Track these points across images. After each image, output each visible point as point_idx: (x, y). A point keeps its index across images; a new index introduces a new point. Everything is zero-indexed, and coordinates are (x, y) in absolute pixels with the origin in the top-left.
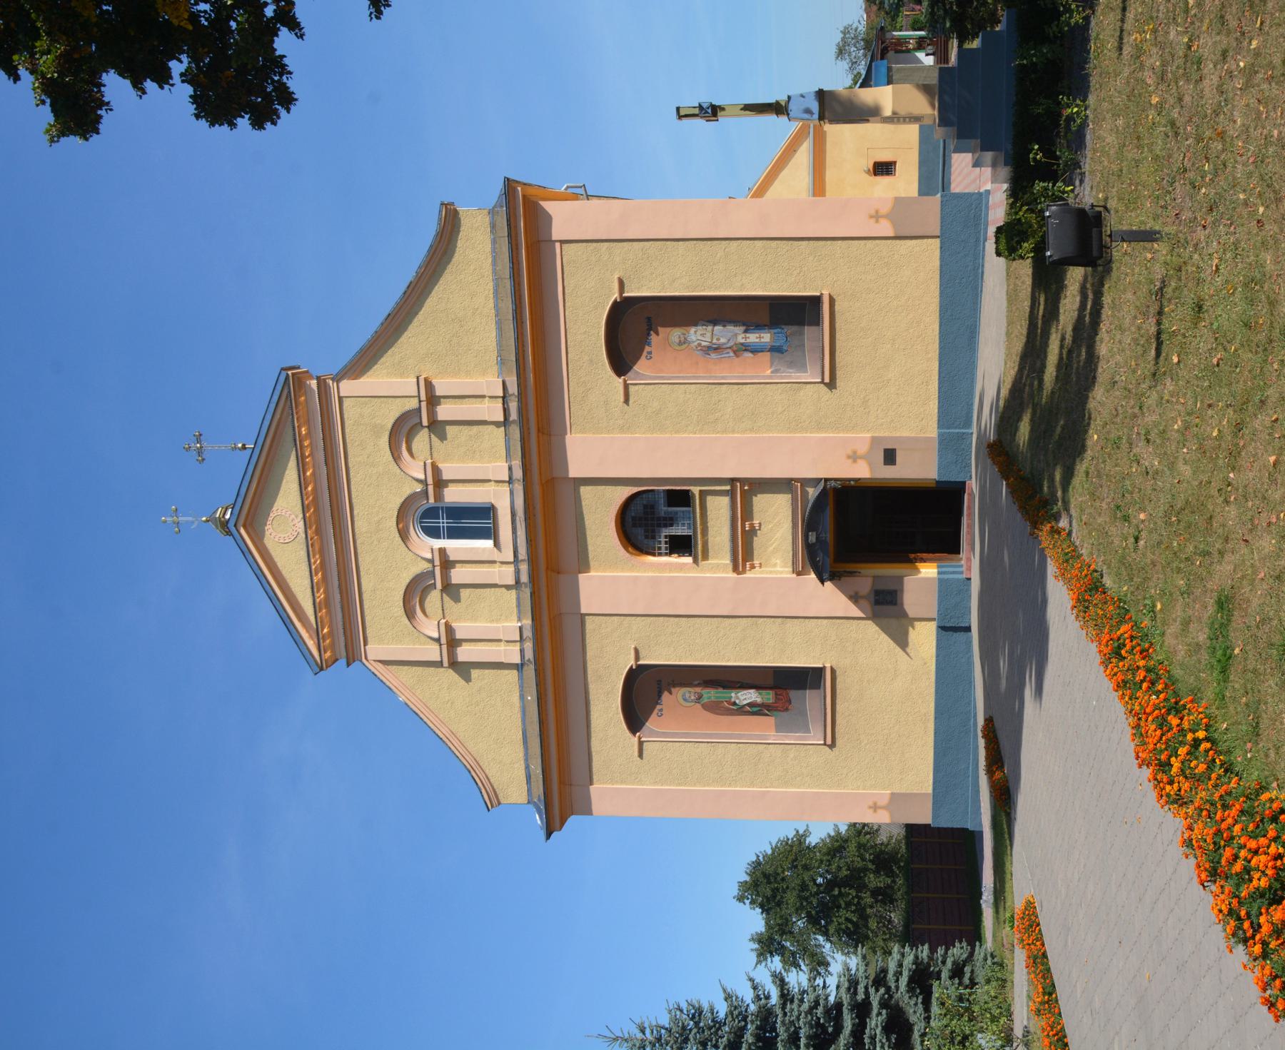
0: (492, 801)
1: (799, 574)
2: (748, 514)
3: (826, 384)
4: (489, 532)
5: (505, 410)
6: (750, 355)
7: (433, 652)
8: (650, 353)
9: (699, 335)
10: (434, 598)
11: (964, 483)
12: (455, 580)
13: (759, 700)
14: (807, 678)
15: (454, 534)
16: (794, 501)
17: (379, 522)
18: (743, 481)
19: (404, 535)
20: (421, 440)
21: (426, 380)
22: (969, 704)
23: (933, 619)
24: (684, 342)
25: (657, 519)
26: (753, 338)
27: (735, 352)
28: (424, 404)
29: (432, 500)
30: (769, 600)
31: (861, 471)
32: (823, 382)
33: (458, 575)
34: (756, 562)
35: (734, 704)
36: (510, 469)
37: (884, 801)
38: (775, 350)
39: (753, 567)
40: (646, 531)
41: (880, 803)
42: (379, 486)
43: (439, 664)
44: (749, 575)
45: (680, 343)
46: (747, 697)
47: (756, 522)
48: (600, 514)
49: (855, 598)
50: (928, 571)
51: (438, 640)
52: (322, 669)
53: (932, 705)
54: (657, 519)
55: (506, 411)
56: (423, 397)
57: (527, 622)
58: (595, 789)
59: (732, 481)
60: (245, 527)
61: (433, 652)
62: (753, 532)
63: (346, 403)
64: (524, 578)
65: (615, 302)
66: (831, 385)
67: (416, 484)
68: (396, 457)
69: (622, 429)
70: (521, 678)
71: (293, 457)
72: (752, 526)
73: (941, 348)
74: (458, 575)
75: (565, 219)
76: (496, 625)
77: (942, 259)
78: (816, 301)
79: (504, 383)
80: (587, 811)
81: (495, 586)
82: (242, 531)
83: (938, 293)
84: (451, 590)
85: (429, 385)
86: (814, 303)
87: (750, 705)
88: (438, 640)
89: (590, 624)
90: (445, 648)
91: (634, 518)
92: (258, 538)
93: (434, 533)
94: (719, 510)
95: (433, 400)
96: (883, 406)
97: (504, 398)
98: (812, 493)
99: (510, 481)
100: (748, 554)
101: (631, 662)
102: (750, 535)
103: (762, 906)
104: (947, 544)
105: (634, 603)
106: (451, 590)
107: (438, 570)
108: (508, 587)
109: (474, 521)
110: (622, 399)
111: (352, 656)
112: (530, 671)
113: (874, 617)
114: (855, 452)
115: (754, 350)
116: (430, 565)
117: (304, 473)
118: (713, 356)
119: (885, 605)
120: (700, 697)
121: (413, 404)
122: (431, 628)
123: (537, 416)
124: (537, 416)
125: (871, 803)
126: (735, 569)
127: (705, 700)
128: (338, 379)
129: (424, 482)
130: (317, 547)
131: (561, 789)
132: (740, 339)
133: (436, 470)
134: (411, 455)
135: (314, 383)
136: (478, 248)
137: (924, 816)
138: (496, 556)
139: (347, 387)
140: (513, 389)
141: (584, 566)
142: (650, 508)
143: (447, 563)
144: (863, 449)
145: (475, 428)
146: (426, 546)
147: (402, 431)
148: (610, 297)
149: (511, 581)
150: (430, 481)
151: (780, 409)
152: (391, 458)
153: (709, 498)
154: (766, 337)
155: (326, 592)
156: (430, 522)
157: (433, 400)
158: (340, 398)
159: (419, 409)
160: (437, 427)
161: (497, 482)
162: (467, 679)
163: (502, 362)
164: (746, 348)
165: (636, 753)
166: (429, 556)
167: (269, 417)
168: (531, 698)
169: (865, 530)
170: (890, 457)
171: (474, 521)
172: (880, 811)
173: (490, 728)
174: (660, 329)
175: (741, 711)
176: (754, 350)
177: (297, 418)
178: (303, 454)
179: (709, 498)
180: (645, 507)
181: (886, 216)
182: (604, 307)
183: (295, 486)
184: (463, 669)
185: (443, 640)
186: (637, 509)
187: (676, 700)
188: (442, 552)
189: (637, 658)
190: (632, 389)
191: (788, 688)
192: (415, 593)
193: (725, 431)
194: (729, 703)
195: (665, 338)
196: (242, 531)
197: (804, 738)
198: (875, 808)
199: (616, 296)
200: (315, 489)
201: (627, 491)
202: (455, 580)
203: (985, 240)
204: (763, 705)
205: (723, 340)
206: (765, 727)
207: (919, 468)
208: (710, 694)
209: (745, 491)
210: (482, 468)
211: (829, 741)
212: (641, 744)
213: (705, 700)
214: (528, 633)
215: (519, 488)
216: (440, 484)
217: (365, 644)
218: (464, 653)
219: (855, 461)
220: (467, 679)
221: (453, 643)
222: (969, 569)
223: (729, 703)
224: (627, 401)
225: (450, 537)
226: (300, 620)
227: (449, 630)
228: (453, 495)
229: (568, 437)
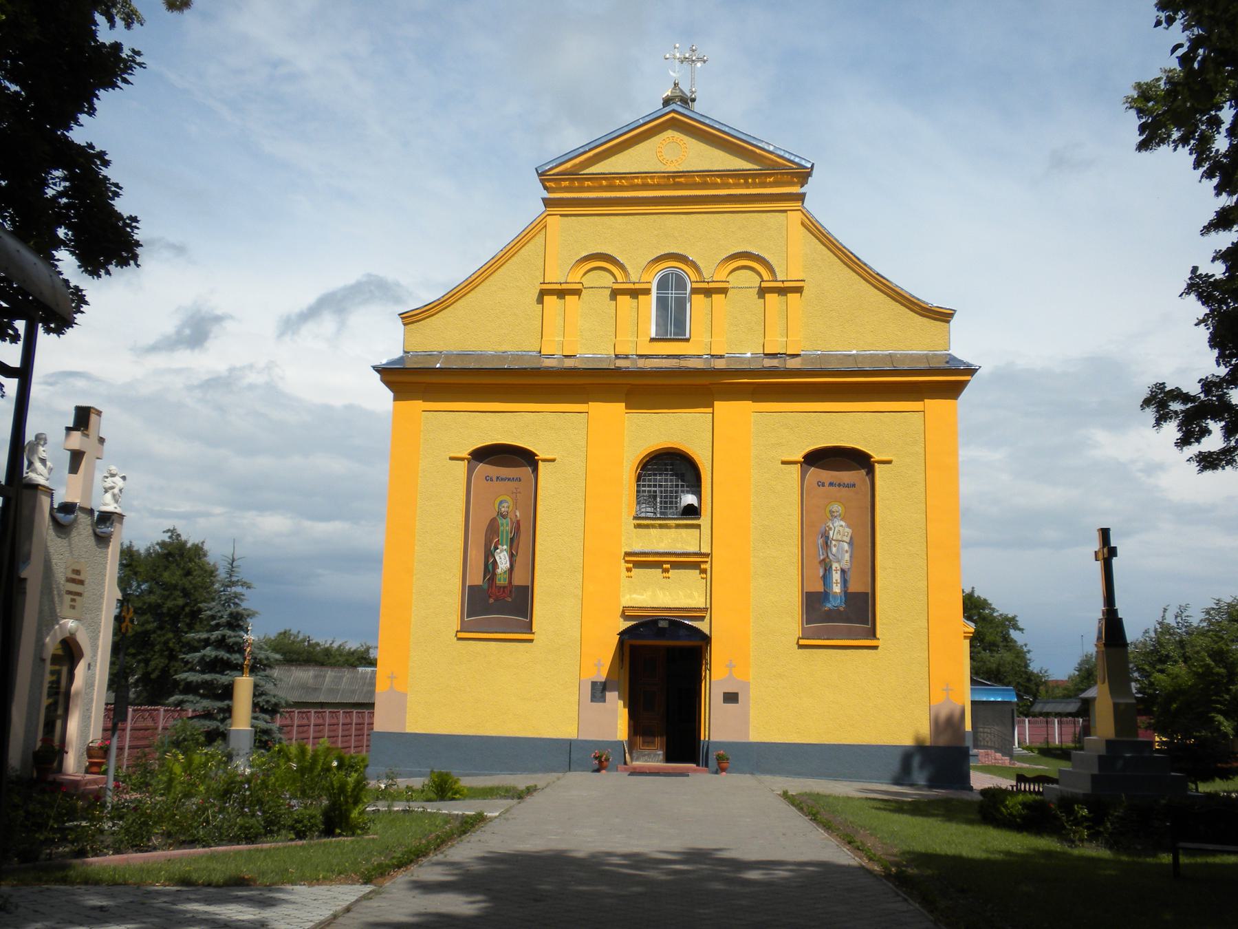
1: (623, 612)
13: (499, 571)
15: (662, 303)
25: (670, 476)
30: (590, 585)
35: (496, 548)
36: (721, 357)
39: (629, 570)
42: (706, 237)
44: (624, 565)
45: (831, 512)
52: (540, 175)
54: (670, 476)
78: (872, 634)
87: (495, 562)
100: (638, 565)
101: (541, 455)
103: (1227, 464)
105: (588, 453)
109: (673, 322)
115: (826, 578)
117: (718, 176)
118: (821, 541)
120: (504, 517)
126: (627, 554)
127: (500, 521)
132: (835, 565)
136: (908, 341)
137: (382, 722)
156: (672, 282)
158: (785, 211)
165: (452, 455)
169: (662, 673)
170: (731, 698)
171: (673, 322)
175: (489, 554)
189: (544, 460)
191: (500, 603)
204: (494, 574)
205: (834, 550)
210: (724, 332)
212: (462, 459)
213: (500, 521)
214: (621, 363)
224: (784, 463)
225: (658, 298)
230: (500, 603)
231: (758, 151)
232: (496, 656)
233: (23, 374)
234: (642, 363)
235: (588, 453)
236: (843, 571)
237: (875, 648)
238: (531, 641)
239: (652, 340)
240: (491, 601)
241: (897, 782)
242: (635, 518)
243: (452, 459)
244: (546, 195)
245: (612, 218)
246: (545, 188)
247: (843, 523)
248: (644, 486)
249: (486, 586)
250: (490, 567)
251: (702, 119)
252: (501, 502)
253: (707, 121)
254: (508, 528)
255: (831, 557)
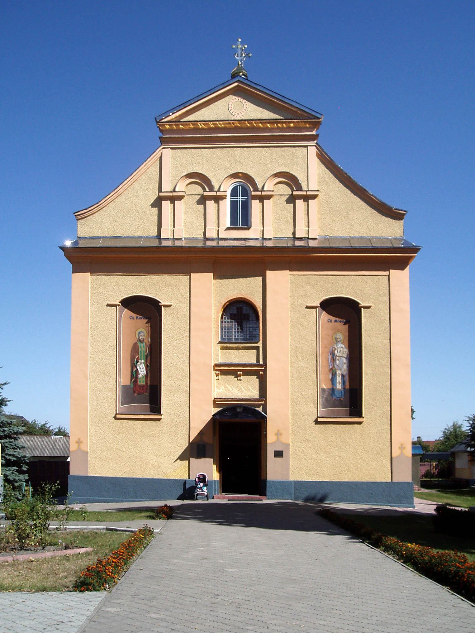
0: (79, 216)
1: (214, 401)
2: (247, 373)
3: (317, 419)
4: (234, 226)
5: (301, 238)
6: (330, 378)
7: (167, 187)
8: (331, 321)
9: (342, 350)
10: (198, 190)
11: (266, 496)
12: (298, 202)
13: (140, 376)
14: (155, 406)
15: (234, 205)
16: (255, 400)
17: (240, 162)
18: (265, 371)
19: (234, 176)
20: (286, 190)
21: (318, 195)
22: (142, 498)
23: (189, 478)
24: (337, 341)
25: (243, 318)
26: (339, 379)
27: (332, 369)
28: (304, 193)
29: (253, 193)
31: (271, 438)
32: (318, 417)
33: (211, 204)
34: (220, 377)
35: (137, 362)
36: (270, 239)
37: (83, 447)
38: (333, 390)
39: (217, 375)
40: (235, 315)
41: (81, 445)
42: (262, 163)
43: (160, 190)
45: (336, 339)
46: (142, 369)
47: (242, 377)
48: (246, 288)
49: (201, 433)
50: (215, 475)
51: (174, 191)
52: (158, 122)
53: (140, 477)
54: (243, 318)
55: (300, 239)
56: (309, 193)
57: (183, 244)
58: (87, 275)
59: (265, 365)
60: (238, 86)
61: (167, 187)
62: (237, 376)
63: (304, 149)
64: (209, 243)
65: (358, 304)
66: (317, 422)
67: (218, 187)
68: (276, 175)
69: (292, 304)
70: (153, 237)
71: (277, 117)
72: (240, 376)
73: (336, 482)
74: (211, 204)
75: (400, 278)
76: (185, 225)
77: (381, 483)
79: (316, 239)
80: (74, 272)
81: (205, 226)
82: (236, 84)
83: (364, 480)
84: (203, 200)
85: (314, 197)
86: (359, 414)
88: (174, 191)
89: (185, 278)
90: (170, 194)
91: (241, 308)
92: (235, 92)
93: (234, 192)
94: (248, 357)
95: (307, 198)
96: (305, 450)
97: (174, 238)
98: (260, 409)
99: (264, 239)
100: (224, 373)
102: (234, 373)
104: (227, 485)
105: (194, 304)
106: (203, 200)
107: (214, 194)
108: (204, 233)
109: (241, 217)
110: (308, 305)
111: (164, 141)
112: (155, 243)
113: (191, 444)
114: (281, 435)
115: (333, 380)
116: (216, 189)
117: (269, 123)
118: (330, 357)
119: (196, 450)
120: (141, 342)
121: (304, 188)
122: (181, 187)
123: (300, 257)
124: (300, 257)
125: (81, 440)
126: (216, 365)
127: (140, 345)
128: (318, 146)
129: (262, 190)
130: (227, 126)
131: (92, 258)
132: (338, 372)
133: (269, 197)
134: (189, 184)
135: (314, 133)
136: (387, 230)
137: (74, 471)
138: (222, 228)
139: (313, 151)
140: (312, 244)
141: (215, 277)
142: (247, 318)
143: (217, 199)
144: (283, 439)
145: (292, 221)
146: (227, 188)
147: (291, 180)
148: (361, 300)
149: (208, 236)
150: (264, 193)
151: (303, 393)
152: (275, 172)
153: (255, 351)
154: (339, 386)
155: (203, 129)
156: (239, 191)
157: (307, 198)
158: (307, 146)
159: (302, 190)
160: (292, 199)
161: (308, 231)
162: (153, 205)
163: (327, 239)
164: (334, 375)
165: (109, 303)
166: (222, 189)
167: (298, 106)
168: (141, 244)
169: (236, 439)
170: (279, 454)
171: (241, 217)
172: (76, 445)
173: (124, 216)
174: (347, 326)
175: (133, 365)
176: (333, 380)
177: (294, 121)
178: (279, 123)
179: (255, 351)
180: (248, 315)
181: (402, 453)
182: (356, 297)
183: (265, 117)
184: (157, 203)
185: (174, 194)
186: (246, 310)
187: (142, 327)
188: (223, 198)
189: (165, 306)
190: (314, 311)
191: (145, 395)
192: (200, 179)
193: (292, 362)
194: (138, 359)
195: (341, 330)
196: (236, 84)
197: (119, 402)
198: (79, 442)
199: (362, 304)
200: (259, 128)
201: (259, 305)
202: (298, 202)
203: (390, 506)
204: (137, 378)
205: (338, 362)
206: (125, 380)
207: (274, 471)
208: (143, 348)
209: (259, 372)
210: (270, 224)
211: (118, 416)
212: (115, 306)
213: (140, 345)
214: (177, 243)
215: (257, 244)
216: (262, 199)
217: (171, 148)
218: (166, 205)
219: (276, 434)
220: (153, 205)
221: (173, 199)
222: (218, 498)
223: (138, 359)
224: (307, 307)
226: (187, 112)
227: (180, 198)
228: (255, 205)
229: (288, 272)
230: (145, 395)
231: (287, 106)
232: (344, 435)
233: (389, 276)
234: (222, 243)
235: (194, 304)
236: (343, 375)
237: (360, 423)
238: (159, 420)
239: (228, 229)
240: (136, 394)
241: (181, 498)
242: (220, 343)
243: (108, 305)
244: (161, 135)
245: (203, 150)
246: (161, 131)
247: (343, 346)
248: (225, 322)
249: (132, 386)
250: (134, 374)
251: (256, 86)
252: (139, 333)
253: (259, 88)
254: (144, 349)
255: (336, 367)
